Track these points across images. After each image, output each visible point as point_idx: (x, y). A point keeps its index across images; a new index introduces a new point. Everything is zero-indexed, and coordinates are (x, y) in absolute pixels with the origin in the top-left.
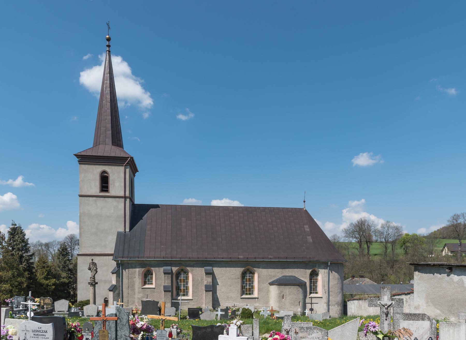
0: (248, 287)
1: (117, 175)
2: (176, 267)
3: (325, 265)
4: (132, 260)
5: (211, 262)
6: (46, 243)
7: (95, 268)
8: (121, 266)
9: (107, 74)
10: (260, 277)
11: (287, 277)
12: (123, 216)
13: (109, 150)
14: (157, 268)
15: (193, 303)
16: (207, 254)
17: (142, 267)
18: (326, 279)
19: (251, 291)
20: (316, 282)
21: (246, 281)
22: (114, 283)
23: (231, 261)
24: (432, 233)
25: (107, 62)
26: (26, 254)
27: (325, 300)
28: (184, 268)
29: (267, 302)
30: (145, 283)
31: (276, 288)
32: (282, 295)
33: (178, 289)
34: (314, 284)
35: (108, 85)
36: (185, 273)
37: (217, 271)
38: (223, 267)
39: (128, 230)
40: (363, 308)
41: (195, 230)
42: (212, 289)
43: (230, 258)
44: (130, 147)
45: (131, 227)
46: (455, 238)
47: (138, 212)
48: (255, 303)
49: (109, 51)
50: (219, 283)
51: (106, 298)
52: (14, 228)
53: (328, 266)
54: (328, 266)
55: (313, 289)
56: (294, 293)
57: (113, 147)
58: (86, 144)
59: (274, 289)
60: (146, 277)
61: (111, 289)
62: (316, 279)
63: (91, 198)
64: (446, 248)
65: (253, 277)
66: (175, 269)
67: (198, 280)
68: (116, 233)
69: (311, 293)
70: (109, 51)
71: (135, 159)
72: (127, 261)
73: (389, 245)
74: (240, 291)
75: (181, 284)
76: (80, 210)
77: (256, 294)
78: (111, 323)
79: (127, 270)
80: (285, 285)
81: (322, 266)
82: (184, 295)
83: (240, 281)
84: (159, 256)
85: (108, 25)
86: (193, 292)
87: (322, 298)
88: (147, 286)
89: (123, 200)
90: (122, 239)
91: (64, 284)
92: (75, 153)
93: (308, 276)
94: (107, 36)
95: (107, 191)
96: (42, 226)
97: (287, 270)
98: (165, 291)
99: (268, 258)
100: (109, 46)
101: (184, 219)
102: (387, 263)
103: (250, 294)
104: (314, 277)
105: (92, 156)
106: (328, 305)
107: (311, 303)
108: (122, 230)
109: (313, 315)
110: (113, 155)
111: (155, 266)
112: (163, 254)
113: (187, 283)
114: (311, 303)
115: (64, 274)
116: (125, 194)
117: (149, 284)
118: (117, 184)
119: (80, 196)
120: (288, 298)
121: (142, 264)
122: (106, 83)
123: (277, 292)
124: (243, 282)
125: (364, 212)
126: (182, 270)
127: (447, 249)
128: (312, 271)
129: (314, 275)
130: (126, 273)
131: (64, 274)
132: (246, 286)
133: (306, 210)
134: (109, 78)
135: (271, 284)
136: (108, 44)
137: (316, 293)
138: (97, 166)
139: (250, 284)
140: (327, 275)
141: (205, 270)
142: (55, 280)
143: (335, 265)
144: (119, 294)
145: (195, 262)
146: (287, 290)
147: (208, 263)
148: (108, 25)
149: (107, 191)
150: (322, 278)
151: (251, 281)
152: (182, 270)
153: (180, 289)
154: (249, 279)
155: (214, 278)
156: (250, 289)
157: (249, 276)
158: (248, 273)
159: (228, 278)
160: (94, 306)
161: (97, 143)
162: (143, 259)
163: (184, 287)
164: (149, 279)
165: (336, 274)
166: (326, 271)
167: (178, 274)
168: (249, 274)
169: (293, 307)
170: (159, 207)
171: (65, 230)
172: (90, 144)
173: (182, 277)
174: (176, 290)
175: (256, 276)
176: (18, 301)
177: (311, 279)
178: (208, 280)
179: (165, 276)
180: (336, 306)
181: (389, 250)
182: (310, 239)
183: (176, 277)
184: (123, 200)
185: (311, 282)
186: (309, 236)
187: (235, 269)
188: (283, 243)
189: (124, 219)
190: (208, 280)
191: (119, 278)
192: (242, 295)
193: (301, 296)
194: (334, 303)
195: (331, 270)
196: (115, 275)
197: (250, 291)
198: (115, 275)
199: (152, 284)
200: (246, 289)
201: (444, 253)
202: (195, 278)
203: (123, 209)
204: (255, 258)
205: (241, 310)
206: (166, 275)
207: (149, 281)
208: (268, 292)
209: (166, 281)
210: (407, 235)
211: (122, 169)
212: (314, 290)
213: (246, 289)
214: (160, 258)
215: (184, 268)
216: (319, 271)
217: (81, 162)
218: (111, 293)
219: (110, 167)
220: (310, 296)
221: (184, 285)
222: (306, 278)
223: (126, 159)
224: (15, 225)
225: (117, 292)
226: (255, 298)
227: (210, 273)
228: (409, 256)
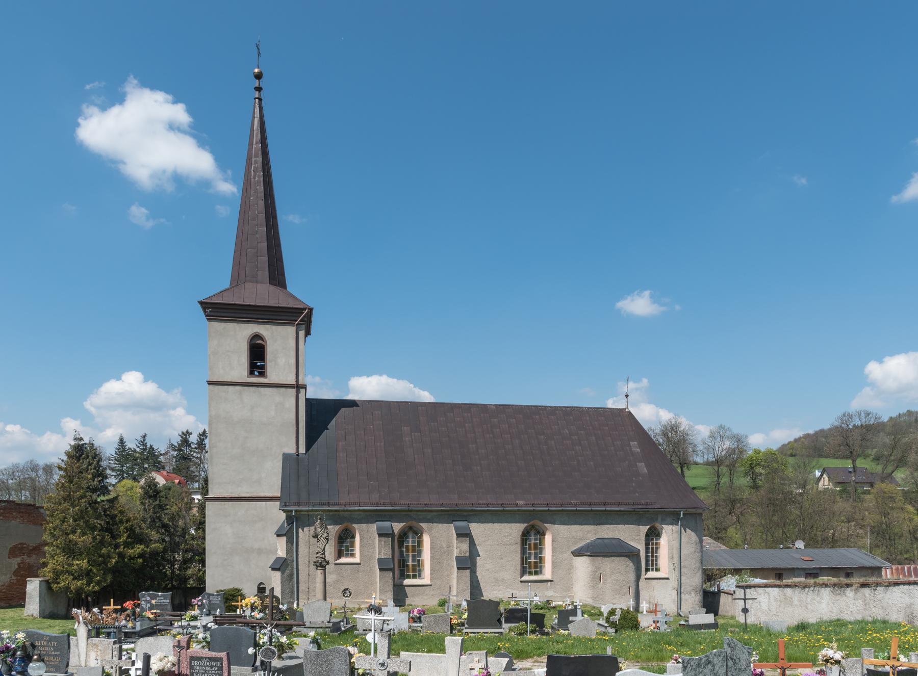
0: (533, 560)
1: (279, 339)
2: (399, 522)
3: (673, 517)
4: (316, 510)
5: (465, 513)
6: (46, 465)
7: (325, 535)
8: (294, 522)
9: (257, 143)
10: (555, 540)
11: (606, 541)
12: (294, 422)
13: (261, 294)
14: (364, 525)
15: (432, 593)
16: (456, 496)
17: (335, 523)
18: (676, 544)
19: (537, 568)
20: (657, 548)
21: (530, 549)
22: (282, 553)
23: (503, 511)
24: (784, 445)
25: (256, 121)
26: (102, 498)
27: (673, 583)
28: (414, 524)
29: (569, 588)
30: (340, 554)
31: (588, 562)
32: (598, 574)
33: (403, 563)
34: (653, 553)
35: (259, 165)
36: (416, 534)
37: (476, 529)
38: (488, 522)
39: (302, 450)
40: (796, 602)
41: (430, 451)
42: (468, 563)
43: (442, 505)
44: (300, 287)
45: (309, 444)
46: (845, 457)
47: (320, 416)
48: (547, 590)
49: (260, 100)
50: (481, 553)
51: (261, 583)
52: (79, 445)
53: (679, 519)
54: (679, 519)
55: (652, 563)
56: (618, 570)
57: (272, 288)
58: (217, 281)
59: (583, 565)
60: (343, 543)
61: (278, 567)
62: (657, 544)
63: (231, 388)
64: (825, 476)
65: (541, 542)
66: (397, 527)
67: (441, 547)
68: (281, 457)
69: (647, 570)
70: (260, 100)
71: (314, 312)
72: (308, 511)
73: (724, 469)
74: (519, 567)
75: (408, 556)
76: (210, 410)
77: (547, 574)
78: (717, 668)
79: (305, 529)
80: (604, 556)
81: (669, 520)
82: (414, 577)
83: (518, 548)
84: (368, 501)
85: (258, 47)
86: (433, 570)
87: (668, 579)
88: (343, 560)
89: (294, 391)
90: (291, 463)
91: (154, 554)
92: (202, 298)
93: (643, 538)
94: (256, 70)
95: (262, 374)
96: (9, 428)
97: (605, 527)
98: (381, 570)
99: (571, 505)
100: (259, 89)
101: (406, 429)
102: (770, 510)
103: (536, 573)
104: (652, 540)
105: (235, 305)
106: (680, 593)
107: (745, 599)
108: (291, 450)
109: (671, 615)
110: (273, 303)
111: (360, 521)
112: (375, 497)
113: (420, 553)
114: (745, 599)
115: (154, 535)
116: (297, 380)
117: (347, 555)
118: (282, 361)
119: (211, 383)
120: (609, 580)
121: (336, 518)
122: (256, 162)
123: (590, 569)
124: (523, 551)
125: (650, 403)
126: (411, 528)
127: (826, 479)
128: (650, 529)
129: (653, 535)
130: (305, 535)
131: (154, 535)
132: (530, 558)
133: (630, 412)
134: (260, 152)
135: (577, 553)
136: (257, 85)
137: (657, 570)
138: (243, 325)
139: (536, 554)
140: (677, 536)
141: (456, 528)
142: (142, 546)
143: (689, 517)
144: (291, 575)
145: (435, 513)
146: (609, 565)
147: (459, 515)
148: (258, 47)
149: (262, 374)
150: (669, 541)
151: (539, 547)
152: (411, 528)
153: (408, 566)
154: (535, 544)
155: (472, 544)
156: (536, 563)
157: (536, 539)
158: (532, 533)
159: (497, 541)
160: (322, 603)
161: (237, 279)
162: (339, 508)
163: (413, 560)
164: (347, 546)
165: (693, 534)
166: (676, 528)
167: (403, 536)
168: (535, 535)
169: (617, 596)
170: (357, 405)
171: (60, 436)
172: (224, 282)
173: (410, 542)
174: (400, 566)
175: (548, 538)
176: (210, 601)
177: (647, 544)
178: (459, 548)
179: (380, 541)
180: (693, 594)
181: (725, 480)
182: (642, 468)
183: (399, 542)
184: (294, 391)
185: (647, 549)
186: (640, 462)
187: (509, 525)
188: (608, 476)
189: (295, 428)
190: (459, 548)
191: (292, 544)
192: (522, 576)
193: (632, 577)
194: (689, 589)
195: (684, 527)
196: (284, 538)
197: (536, 567)
198: (284, 538)
199: (352, 555)
200: (530, 564)
201: (821, 484)
202: (436, 543)
203: (294, 410)
204: (547, 505)
205: (618, 612)
206: (383, 539)
207: (347, 550)
208: (570, 569)
209: (380, 549)
210: (757, 452)
211: (291, 330)
212: (653, 565)
213: (530, 564)
214: (370, 505)
215: (414, 524)
216: (662, 529)
217: (210, 317)
218: (278, 574)
219: (268, 326)
220: (647, 576)
221: (413, 556)
222: (638, 541)
223: (299, 311)
224: (81, 439)
225: (287, 572)
226: (547, 581)
227: (464, 534)
228: (762, 492)
